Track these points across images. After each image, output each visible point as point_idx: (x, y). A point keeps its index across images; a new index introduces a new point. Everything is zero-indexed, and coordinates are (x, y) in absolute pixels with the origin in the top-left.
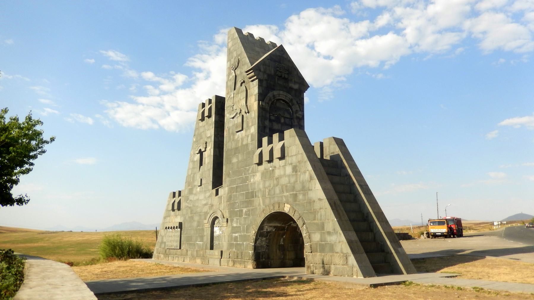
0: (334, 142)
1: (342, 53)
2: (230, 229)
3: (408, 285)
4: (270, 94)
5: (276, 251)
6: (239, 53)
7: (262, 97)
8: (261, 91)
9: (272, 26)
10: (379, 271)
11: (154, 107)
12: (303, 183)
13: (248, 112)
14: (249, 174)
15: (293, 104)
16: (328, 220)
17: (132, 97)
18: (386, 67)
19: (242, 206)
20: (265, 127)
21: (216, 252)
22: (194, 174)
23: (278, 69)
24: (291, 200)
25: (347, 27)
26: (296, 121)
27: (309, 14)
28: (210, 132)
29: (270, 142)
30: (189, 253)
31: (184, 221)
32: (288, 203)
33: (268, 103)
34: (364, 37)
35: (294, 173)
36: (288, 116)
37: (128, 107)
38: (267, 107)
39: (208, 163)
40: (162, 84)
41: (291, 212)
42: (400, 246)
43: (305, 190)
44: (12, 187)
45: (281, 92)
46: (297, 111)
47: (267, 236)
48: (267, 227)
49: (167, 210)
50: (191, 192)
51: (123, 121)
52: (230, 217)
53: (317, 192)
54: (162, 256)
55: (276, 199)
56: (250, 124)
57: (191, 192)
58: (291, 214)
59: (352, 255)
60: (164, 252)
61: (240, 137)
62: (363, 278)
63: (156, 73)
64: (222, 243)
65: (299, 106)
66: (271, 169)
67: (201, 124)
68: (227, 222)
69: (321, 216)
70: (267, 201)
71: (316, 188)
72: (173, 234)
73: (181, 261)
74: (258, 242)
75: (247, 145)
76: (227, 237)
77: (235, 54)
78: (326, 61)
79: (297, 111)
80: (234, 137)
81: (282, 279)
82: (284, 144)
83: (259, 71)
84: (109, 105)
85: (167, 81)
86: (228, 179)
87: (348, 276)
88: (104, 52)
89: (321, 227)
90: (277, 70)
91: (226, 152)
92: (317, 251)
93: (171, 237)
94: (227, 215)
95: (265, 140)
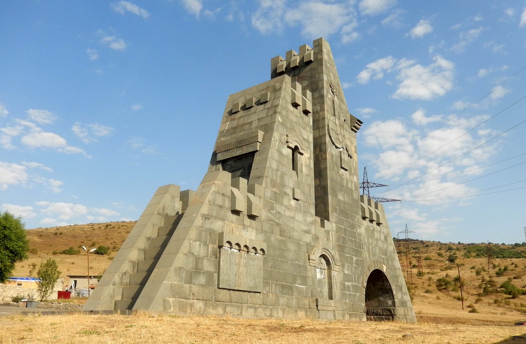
44: (12, 267)
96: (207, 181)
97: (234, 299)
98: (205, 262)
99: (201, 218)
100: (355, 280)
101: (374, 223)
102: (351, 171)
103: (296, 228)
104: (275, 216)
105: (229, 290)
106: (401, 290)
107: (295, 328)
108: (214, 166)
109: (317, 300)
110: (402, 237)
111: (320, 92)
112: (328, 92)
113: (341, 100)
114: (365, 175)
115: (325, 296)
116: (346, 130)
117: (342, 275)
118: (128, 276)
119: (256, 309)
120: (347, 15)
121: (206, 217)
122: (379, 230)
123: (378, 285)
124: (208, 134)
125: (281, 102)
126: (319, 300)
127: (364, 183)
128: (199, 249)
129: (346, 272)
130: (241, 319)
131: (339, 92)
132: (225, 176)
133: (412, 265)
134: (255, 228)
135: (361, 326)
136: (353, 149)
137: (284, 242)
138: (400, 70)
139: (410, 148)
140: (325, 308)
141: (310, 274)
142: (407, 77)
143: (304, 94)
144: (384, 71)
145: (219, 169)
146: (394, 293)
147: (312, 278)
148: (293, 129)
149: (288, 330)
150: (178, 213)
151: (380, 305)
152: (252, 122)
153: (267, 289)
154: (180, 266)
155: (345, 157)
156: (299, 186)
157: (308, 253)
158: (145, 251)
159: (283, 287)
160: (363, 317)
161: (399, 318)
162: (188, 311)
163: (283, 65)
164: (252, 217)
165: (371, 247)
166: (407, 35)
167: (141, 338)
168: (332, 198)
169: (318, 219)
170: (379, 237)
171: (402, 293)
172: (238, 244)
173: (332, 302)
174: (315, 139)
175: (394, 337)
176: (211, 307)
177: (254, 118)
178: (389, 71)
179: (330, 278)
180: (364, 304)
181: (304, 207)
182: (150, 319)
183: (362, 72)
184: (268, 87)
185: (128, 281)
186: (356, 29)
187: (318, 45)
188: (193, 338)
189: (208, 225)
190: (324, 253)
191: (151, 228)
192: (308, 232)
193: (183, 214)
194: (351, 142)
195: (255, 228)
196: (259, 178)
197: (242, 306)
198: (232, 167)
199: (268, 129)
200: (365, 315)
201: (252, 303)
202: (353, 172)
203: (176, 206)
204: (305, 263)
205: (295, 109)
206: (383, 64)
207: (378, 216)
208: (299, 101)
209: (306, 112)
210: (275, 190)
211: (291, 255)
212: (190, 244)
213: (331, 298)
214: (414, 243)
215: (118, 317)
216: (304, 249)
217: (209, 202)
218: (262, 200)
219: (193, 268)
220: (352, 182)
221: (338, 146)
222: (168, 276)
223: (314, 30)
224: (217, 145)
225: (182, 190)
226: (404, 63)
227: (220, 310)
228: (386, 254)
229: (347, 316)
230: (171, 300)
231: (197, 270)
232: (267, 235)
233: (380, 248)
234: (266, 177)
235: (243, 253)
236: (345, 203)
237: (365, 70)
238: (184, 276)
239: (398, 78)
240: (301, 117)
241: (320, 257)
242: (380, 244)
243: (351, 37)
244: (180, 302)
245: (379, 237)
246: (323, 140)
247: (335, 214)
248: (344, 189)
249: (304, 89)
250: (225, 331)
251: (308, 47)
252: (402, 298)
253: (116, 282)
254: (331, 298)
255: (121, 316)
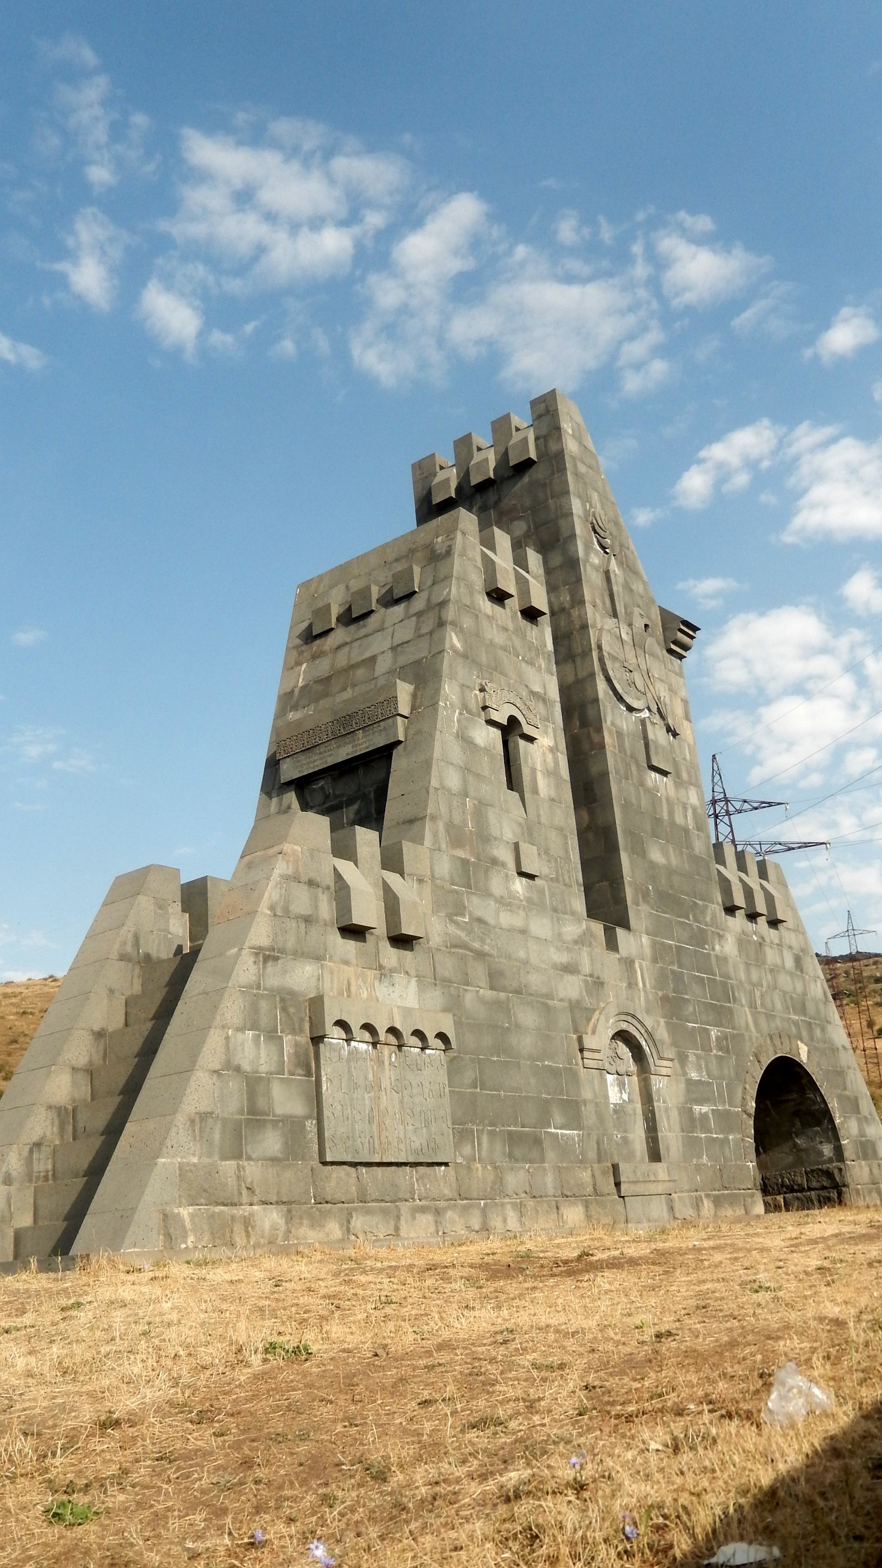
96: (260, 845)
97: (373, 1192)
98: (277, 1091)
99: (252, 959)
100: (721, 1095)
101: (762, 921)
102: (678, 775)
103: (534, 960)
104: (470, 932)
105: (354, 1165)
106: (856, 1109)
107: (566, 1262)
108: (275, 800)
109: (615, 1168)
110: (840, 949)
111: (564, 551)
112: (588, 547)
113: (629, 567)
114: (717, 778)
115: (638, 1154)
116: (652, 655)
117: (682, 1086)
118: (46, 1151)
119: (438, 1212)
120: (631, 309)
121: (268, 956)
122: (776, 941)
123: (787, 1102)
124: (240, 707)
125: (454, 590)
126: (622, 1167)
127: (714, 802)
128: (254, 1053)
129: (694, 1075)
130: (400, 1250)
131: (621, 546)
132: (315, 827)
133: (876, 1028)
134: (413, 972)
135: (757, 1235)
136: (679, 711)
137: (503, 1007)
138: (796, 459)
139: (845, 684)
140: (640, 1189)
141: (587, 1094)
142: (819, 476)
143: (520, 561)
144: (751, 465)
145: (289, 807)
146: (837, 1121)
147: (597, 1105)
148: (496, 668)
149: (545, 1272)
150: (180, 948)
151: (799, 1161)
152: (373, 659)
153: (467, 1150)
154: (202, 1108)
155: (658, 734)
156: (530, 834)
157: (576, 1031)
158: (91, 1072)
159: (512, 1139)
160: (754, 1202)
161: (858, 1192)
162: (240, 1239)
163: (448, 480)
164: (402, 941)
165: (758, 994)
166: (808, 353)
167: (113, 1339)
168: (632, 862)
169: (598, 928)
170: (779, 961)
171: (859, 1120)
172: (368, 1027)
173: (660, 1170)
174: (565, 690)
175: (861, 1258)
176: (305, 1222)
177: (379, 645)
178: (766, 464)
179: (647, 1097)
180: (752, 1165)
181: (552, 895)
182: (131, 1278)
183: (687, 475)
184: (412, 551)
185: (50, 1167)
186: (659, 351)
187: (546, 410)
188: (268, 1323)
189: (274, 977)
190: (624, 1026)
191: (105, 1001)
192: (570, 969)
193: (195, 952)
194: (671, 689)
195: (413, 972)
196: (411, 822)
197: (398, 1209)
198: (327, 797)
199: (425, 675)
200: (759, 1195)
201: (426, 1198)
202: (685, 775)
203: (172, 929)
204: (570, 1063)
205: (497, 608)
206: (747, 443)
207: (770, 900)
208: (508, 585)
209: (531, 614)
210: (461, 853)
211: (526, 1043)
212: (223, 1045)
213: (655, 1155)
214: (875, 963)
215: (31, 1280)
216: (565, 1020)
217: (272, 908)
218: (427, 889)
219: (241, 1112)
220: (685, 808)
221: (635, 704)
222: (169, 1143)
223: (542, 364)
224: (278, 735)
225: (185, 879)
226: (806, 437)
227: (334, 1229)
228: (803, 1011)
229: (707, 1205)
230: (185, 1212)
231: (255, 1117)
232: (451, 989)
233: (785, 993)
234: (434, 818)
235: (386, 1050)
236: (670, 871)
237: (694, 468)
238: (217, 1136)
239: (792, 481)
240: (517, 630)
241: (613, 1038)
242: (784, 981)
243: (647, 374)
244: (212, 1216)
245: (779, 961)
246: (590, 690)
247: (644, 908)
248: (661, 829)
249: (518, 546)
250: (360, 1292)
251: (516, 421)
252: (862, 1134)
253: (14, 1174)
254: (655, 1155)
255: (43, 1275)
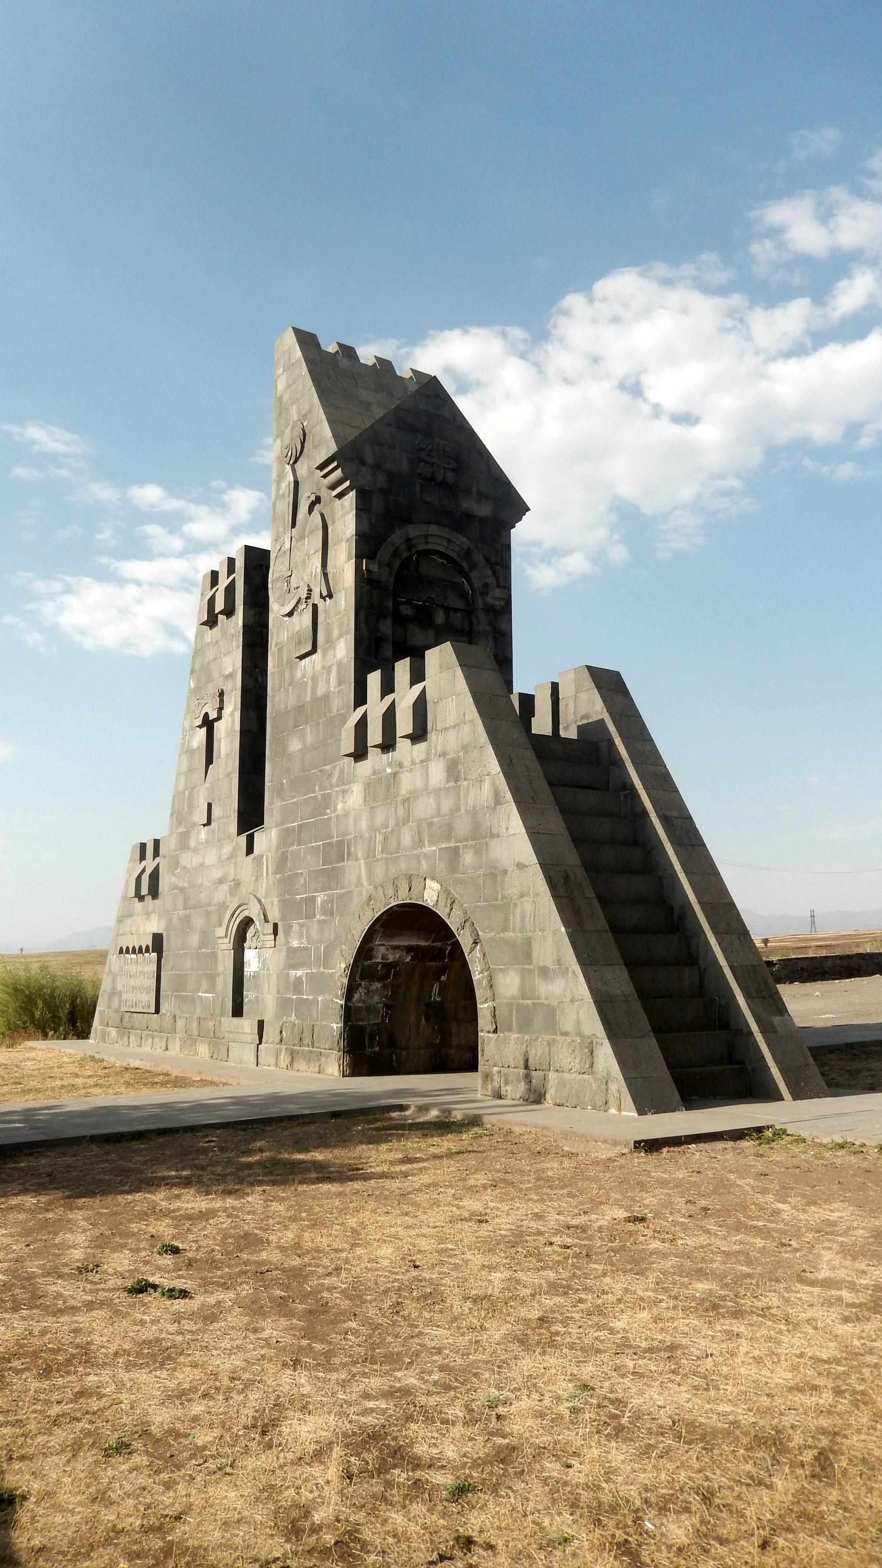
0: (589, 683)
1: (727, 403)
2: (284, 954)
3: (770, 1141)
4: (397, 538)
5: (418, 1025)
6: (305, 408)
7: (367, 545)
8: (366, 528)
9: (509, 329)
10: (694, 1092)
11: (171, 588)
12: (474, 813)
13: (330, 596)
14: (331, 787)
15: (473, 567)
16: (543, 930)
17: (104, 560)
18: (865, 442)
19: (313, 886)
20: (379, 641)
21: (247, 1025)
22: (192, 789)
23: (422, 455)
24: (441, 866)
25: (741, 320)
26: (482, 617)
27: (623, 285)
28: (232, 662)
29: (388, 687)
30: (180, 1024)
31: (167, 929)
32: (433, 879)
33: (389, 565)
34: (797, 351)
35: (452, 784)
36: (458, 604)
37: (95, 592)
38: (387, 578)
39: (227, 755)
40: (190, 519)
41: (441, 904)
42: (781, 1009)
43: (481, 835)
45: (433, 529)
46: (486, 586)
47: (386, 977)
48: (382, 949)
49: (125, 898)
50: (184, 839)
51: (83, 633)
52: (284, 918)
53: (513, 842)
54: (113, 1032)
55: (403, 866)
56: (335, 633)
57: (184, 839)
58: (442, 912)
59: (606, 1042)
60: (118, 1021)
61: (310, 672)
62: (636, 1115)
63: (171, 492)
64: (263, 998)
65: (495, 572)
66: (389, 770)
67: (210, 635)
68: (275, 933)
69: (523, 918)
70: (379, 870)
71: (511, 831)
72: (140, 968)
73: (159, 1050)
74: (356, 996)
75: (327, 697)
76: (274, 978)
77: (294, 414)
78: (677, 430)
79: (486, 586)
80: (292, 676)
81: (394, 1115)
82: (424, 691)
83: (353, 460)
84: (40, 586)
85: (202, 511)
86: (278, 803)
87: (594, 1108)
88: (14, 429)
89: (523, 953)
90: (420, 460)
91: (274, 719)
92: (510, 1029)
93: (135, 976)
94: (274, 914)
95: (374, 679)
